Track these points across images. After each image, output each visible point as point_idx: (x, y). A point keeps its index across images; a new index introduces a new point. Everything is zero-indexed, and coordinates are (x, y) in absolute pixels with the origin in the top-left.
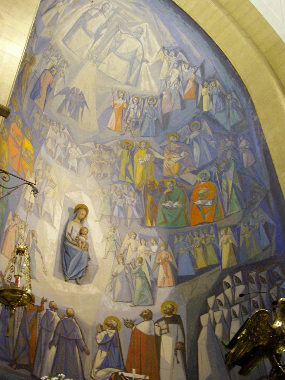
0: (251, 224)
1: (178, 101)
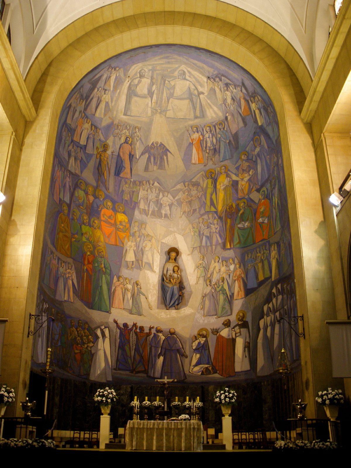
1: (240, 119)
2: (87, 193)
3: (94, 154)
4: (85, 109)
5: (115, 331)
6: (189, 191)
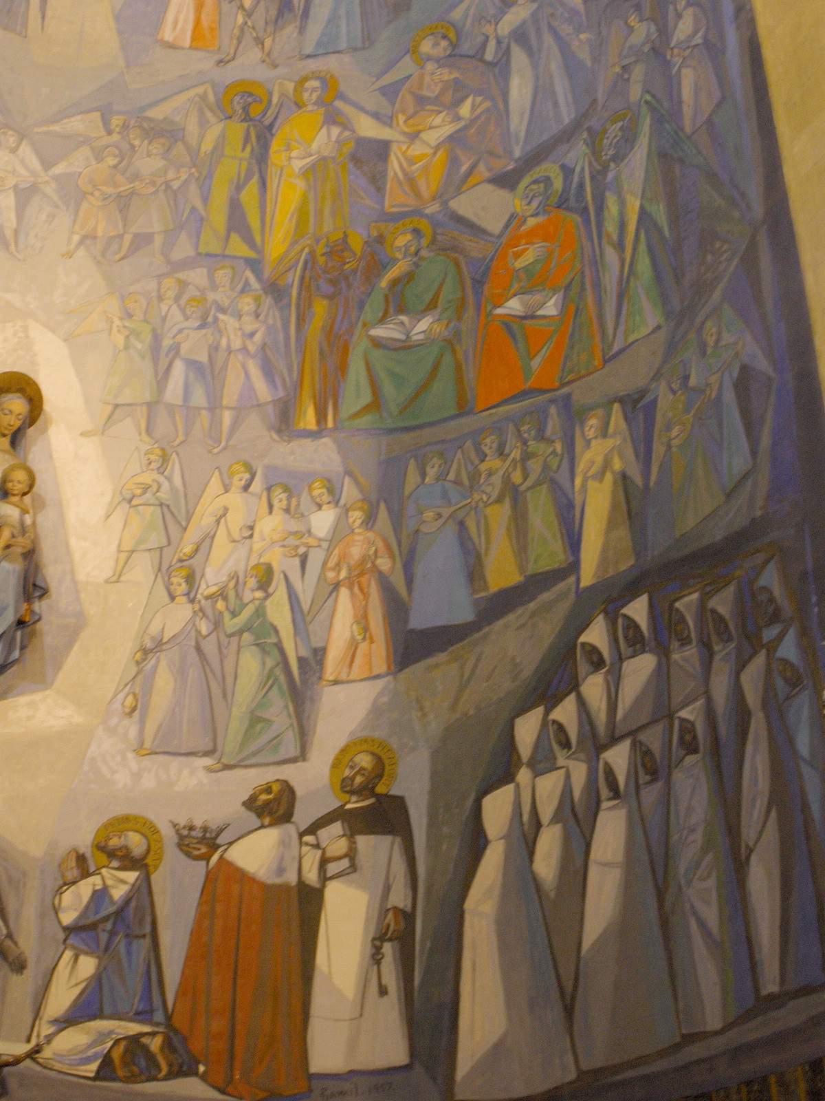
0: (693, 382)
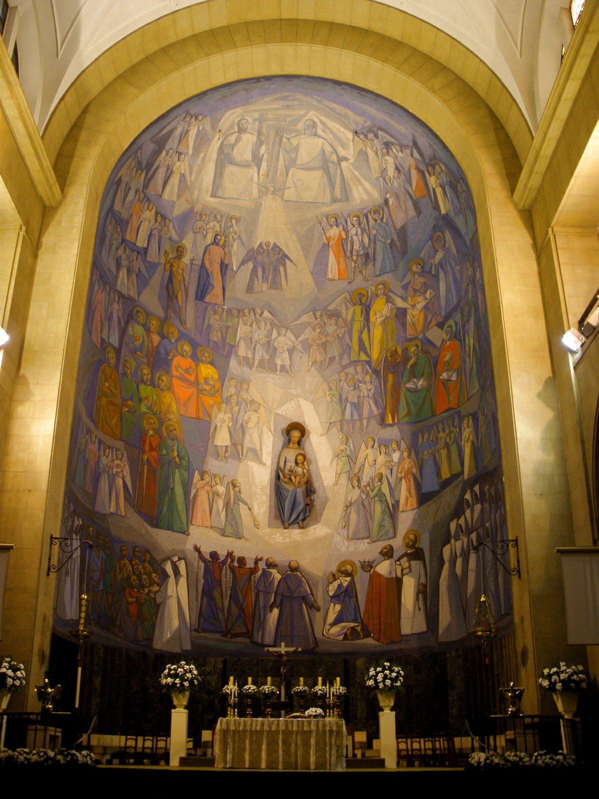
1: (409, 203)
2: (148, 330)
3: (161, 264)
4: (146, 186)
5: (196, 565)
6: (323, 326)
